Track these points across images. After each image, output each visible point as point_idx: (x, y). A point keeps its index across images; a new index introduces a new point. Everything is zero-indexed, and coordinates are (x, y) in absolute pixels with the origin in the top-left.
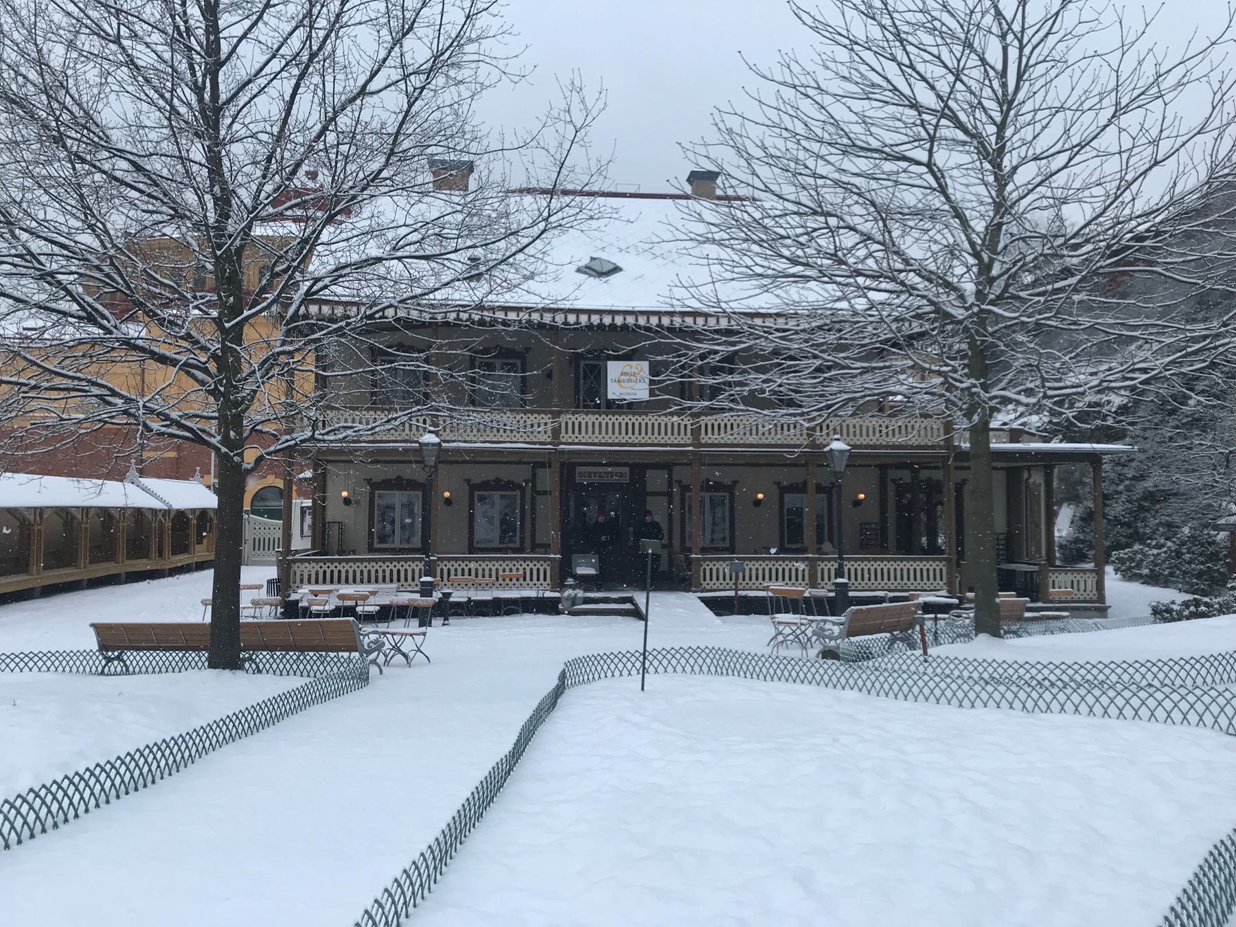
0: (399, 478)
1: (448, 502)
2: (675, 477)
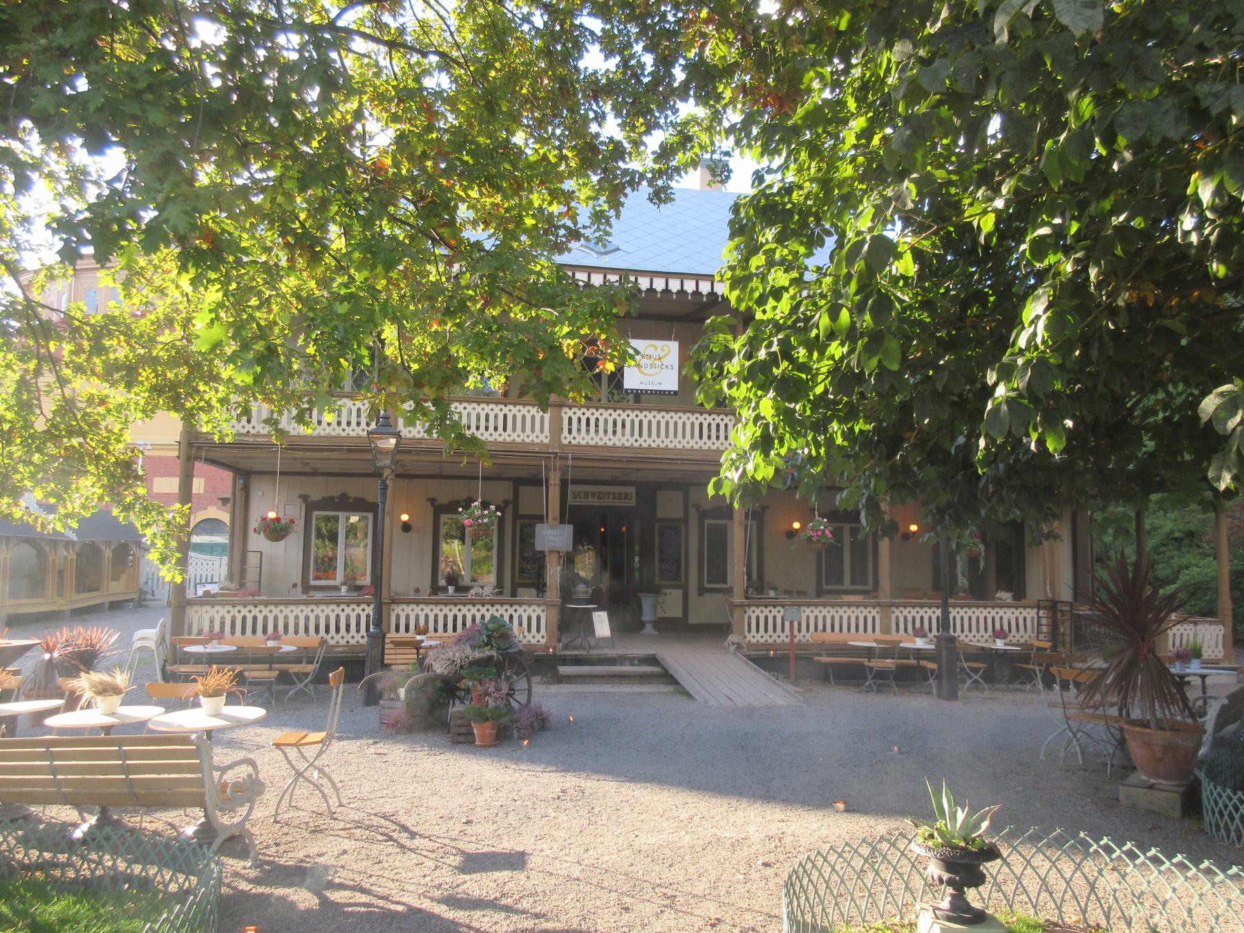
0: (344, 497)
1: (406, 527)
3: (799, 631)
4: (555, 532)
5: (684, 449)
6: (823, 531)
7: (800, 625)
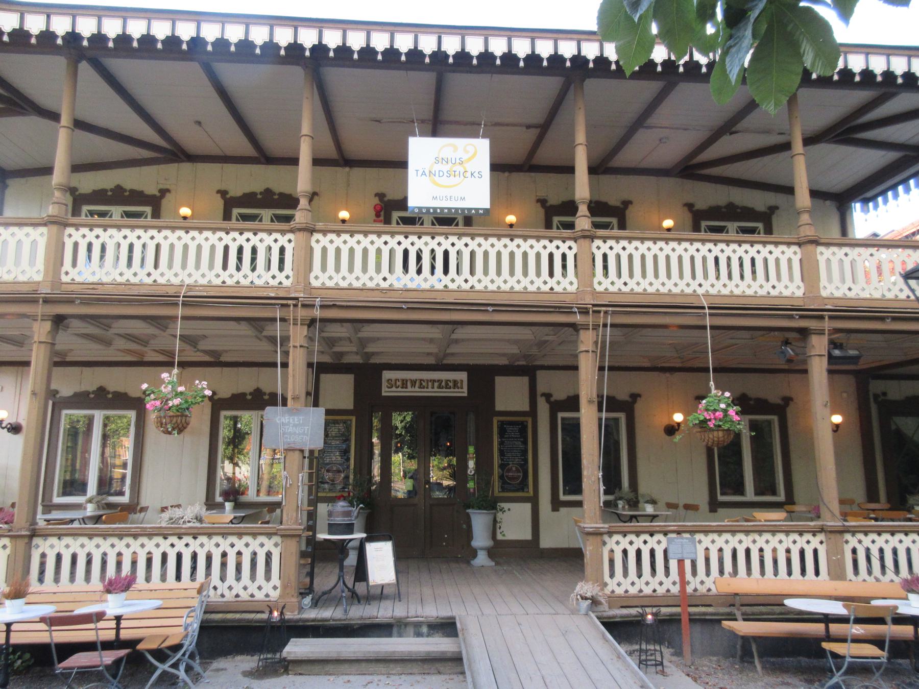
0: (101, 390)
2: (541, 388)
3: (694, 573)
4: (296, 419)
5: (499, 291)
6: (725, 411)
7: (694, 564)
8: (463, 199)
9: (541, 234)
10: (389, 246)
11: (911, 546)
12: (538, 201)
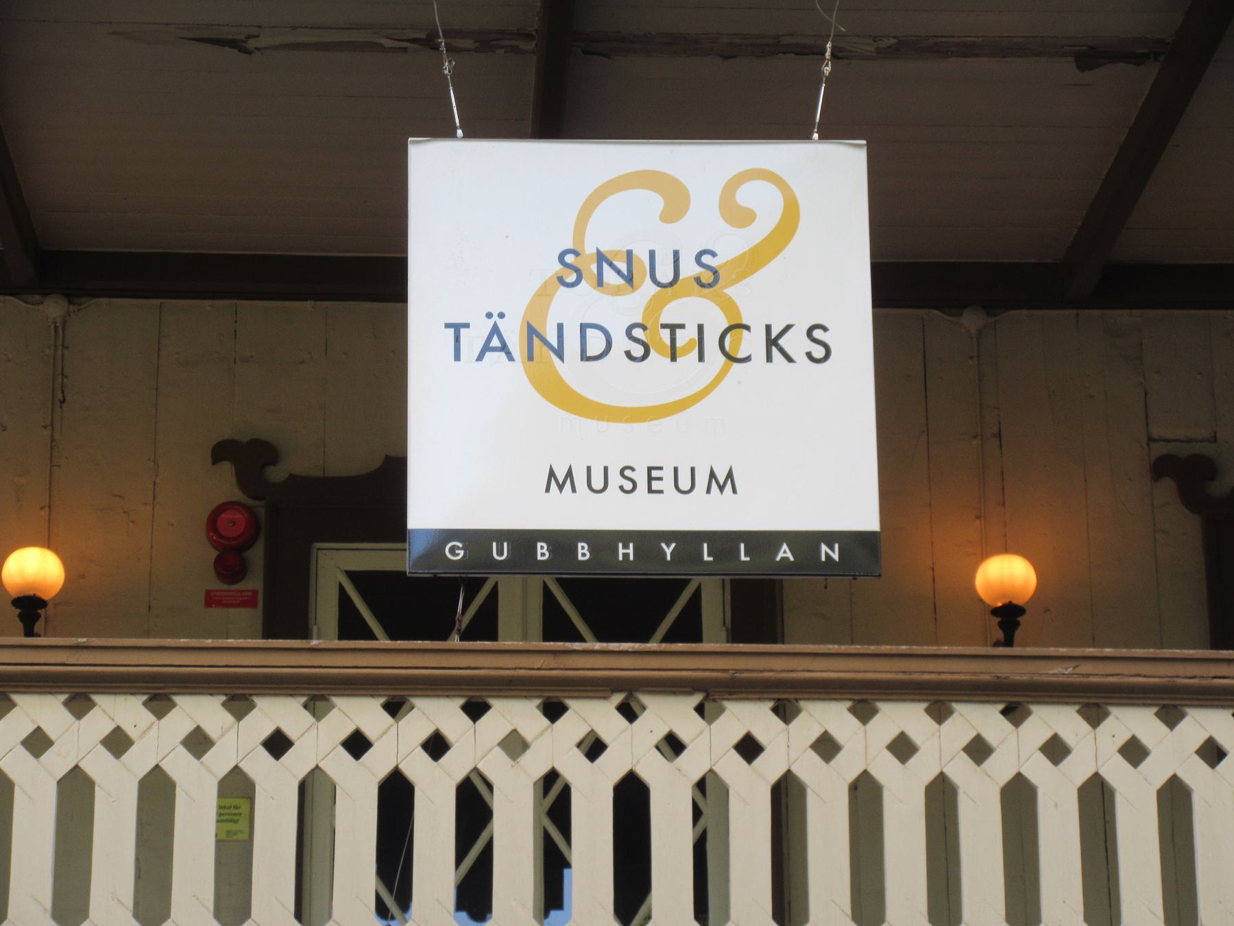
8: (724, 482)
9: (1186, 675)
10: (297, 763)
11: (1196, 774)
12: (1162, 468)
